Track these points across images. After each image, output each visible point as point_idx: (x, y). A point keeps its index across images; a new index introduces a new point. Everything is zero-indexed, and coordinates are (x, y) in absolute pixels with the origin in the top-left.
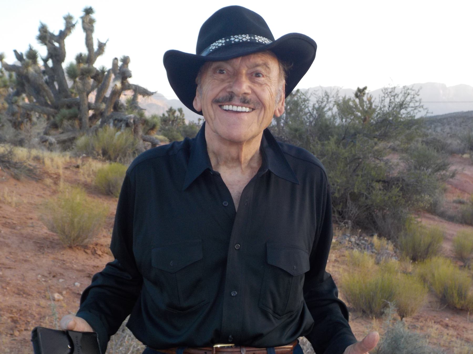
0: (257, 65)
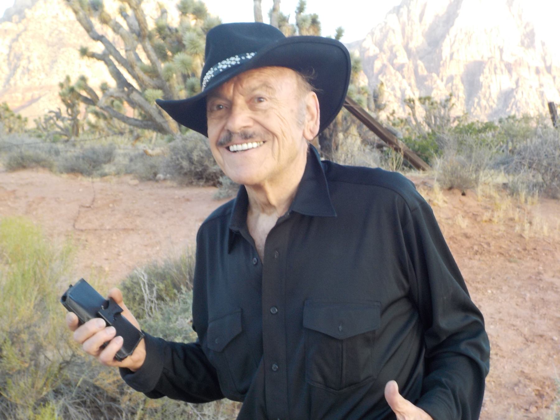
0: (254, 89)
